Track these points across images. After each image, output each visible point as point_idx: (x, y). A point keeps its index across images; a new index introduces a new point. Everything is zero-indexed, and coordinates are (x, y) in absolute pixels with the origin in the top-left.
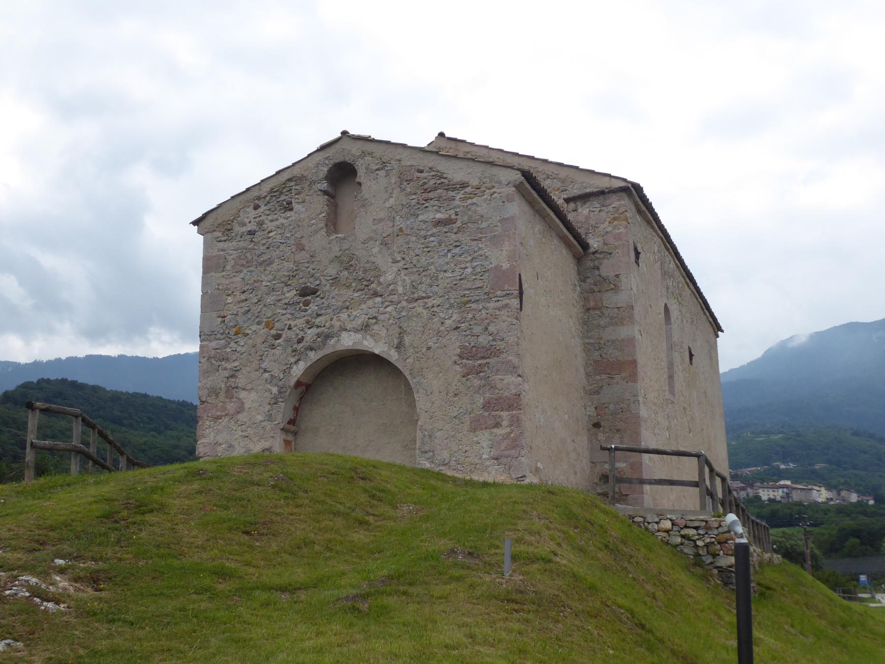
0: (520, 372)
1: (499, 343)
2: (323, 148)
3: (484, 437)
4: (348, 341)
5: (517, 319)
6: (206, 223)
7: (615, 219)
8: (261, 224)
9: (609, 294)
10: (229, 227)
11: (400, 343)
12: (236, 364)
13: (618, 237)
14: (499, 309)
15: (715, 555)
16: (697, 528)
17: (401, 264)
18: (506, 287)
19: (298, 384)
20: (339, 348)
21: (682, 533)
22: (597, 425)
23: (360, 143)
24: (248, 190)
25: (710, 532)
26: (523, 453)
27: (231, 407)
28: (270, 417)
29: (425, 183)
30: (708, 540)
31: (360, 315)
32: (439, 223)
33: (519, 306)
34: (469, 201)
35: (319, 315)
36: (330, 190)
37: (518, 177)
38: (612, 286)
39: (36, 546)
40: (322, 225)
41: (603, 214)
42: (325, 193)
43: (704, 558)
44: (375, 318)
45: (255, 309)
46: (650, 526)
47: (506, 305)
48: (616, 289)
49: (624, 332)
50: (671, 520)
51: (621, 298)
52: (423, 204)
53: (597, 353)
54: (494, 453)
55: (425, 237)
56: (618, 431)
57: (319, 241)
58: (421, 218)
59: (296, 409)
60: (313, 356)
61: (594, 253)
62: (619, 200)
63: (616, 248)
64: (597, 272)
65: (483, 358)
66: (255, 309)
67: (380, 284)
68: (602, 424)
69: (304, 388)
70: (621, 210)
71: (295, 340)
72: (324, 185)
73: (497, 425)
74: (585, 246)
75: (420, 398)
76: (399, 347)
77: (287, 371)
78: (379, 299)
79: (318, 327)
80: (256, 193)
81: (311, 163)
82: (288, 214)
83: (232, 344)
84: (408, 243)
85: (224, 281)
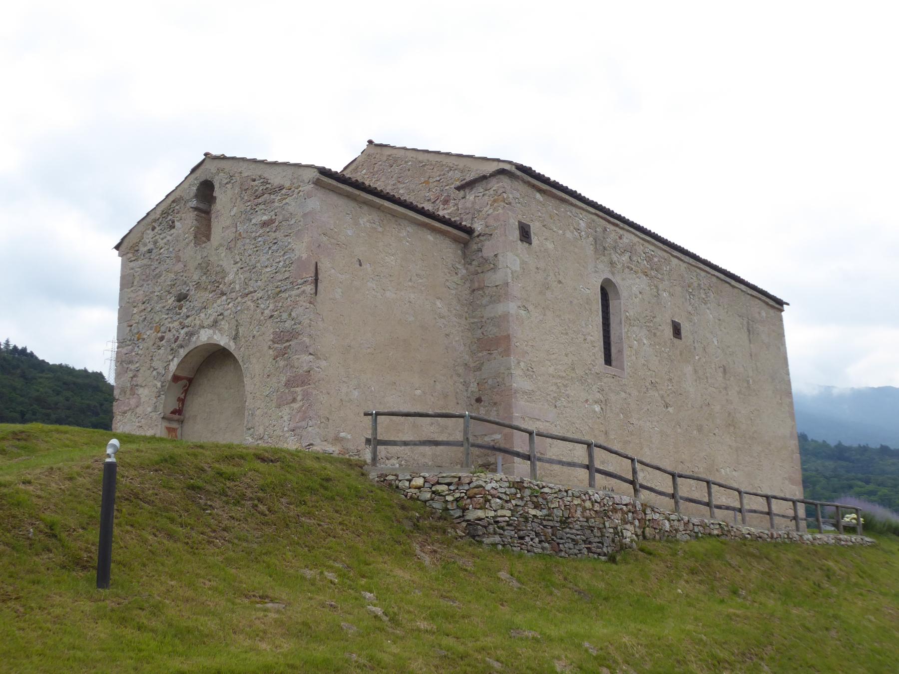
0: (311, 351)
1: (298, 326)
2: (194, 170)
3: (285, 411)
4: (204, 336)
5: (310, 303)
6: (122, 248)
7: (495, 201)
8: (155, 243)
9: (490, 273)
10: (136, 248)
11: (237, 334)
12: (138, 365)
13: (497, 219)
14: (299, 296)
15: (464, 509)
16: (449, 484)
17: (239, 265)
18: (304, 275)
19: (176, 378)
20: (199, 344)
21: (433, 489)
22: (479, 400)
23: (216, 161)
24: (148, 214)
25: (460, 488)
26: (310, 423)
27: (133, 402)
28: (155, 409)
29: (257, 190)
30: (457, 495)
31: (213, 312)
32: (265, 224)
33: (314, 291)
34: (284, 202)
35: (188, 317)
36: (201, 206)
37: (316, 174)
38: (492, 266)
39: (733, 617)
40: (192, 238)
41: (486, 197)
42: (196, 209)
43: (452, 512)
44: (221, 314)
45: (149, 317)
46: (400, 484)
47: (304, 292)
48: (495, 269)
49: (500, 309)
50: (424, 478)
51: (497, 278)
52: (254, 210)
53: (480, 331)
54: (292, 426)
55: (255, 239)
56: (495, 404)
57: (191, 254)
58: (254, 221)
59: (182, 401)
60: (183, 352)
61: (478, 236)
62: (498, 183)
63: (496, 228)
64: (480, 254)
65: (287, 341)
66: (149, 317)
67: (225, 284)
68: (483, 398)
69: (185, 382)
70: (500, 192)
71: (173, 340)
72: (194, 203)
73: (294, 400)
74: (469, 231)
75: (247, 380)
76: (235, 338)
77: (166, 368)
78: (224, 297)
79: (188, 327)
80: (152, 217)
81: (186, 185)
82: (173, 231)
83: (136, 349)
84: (244, 245)
85: (133, 295)
